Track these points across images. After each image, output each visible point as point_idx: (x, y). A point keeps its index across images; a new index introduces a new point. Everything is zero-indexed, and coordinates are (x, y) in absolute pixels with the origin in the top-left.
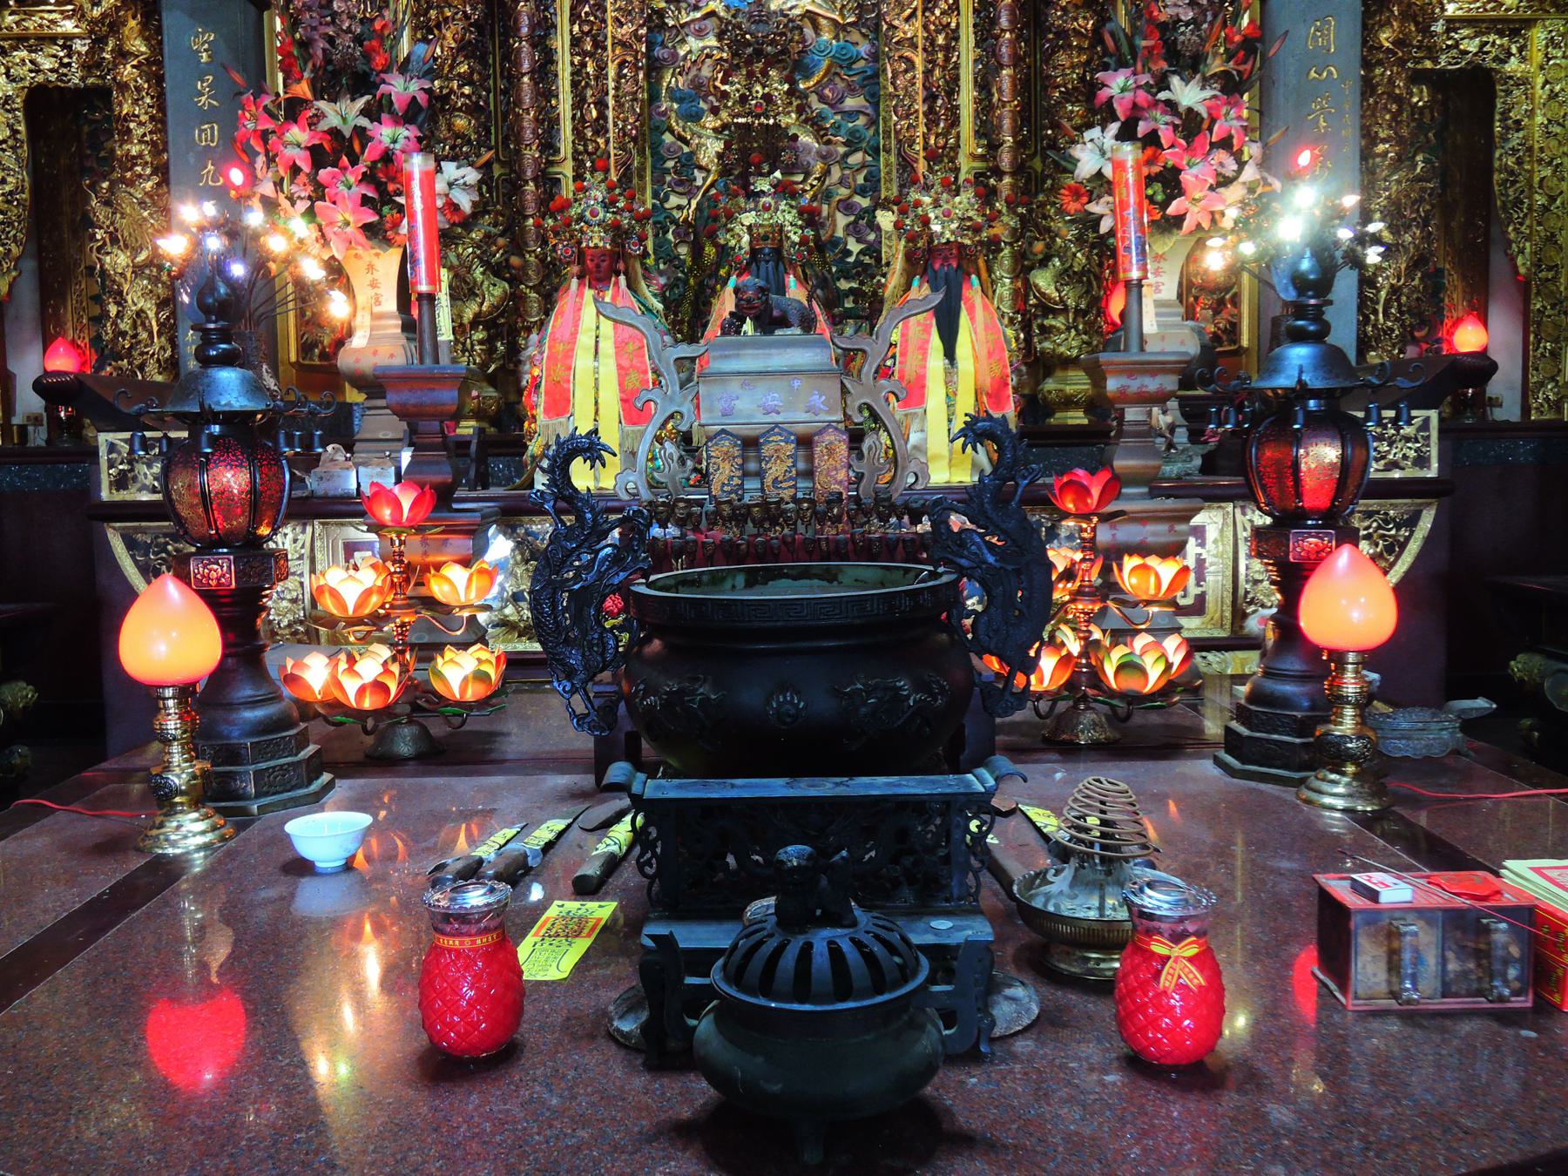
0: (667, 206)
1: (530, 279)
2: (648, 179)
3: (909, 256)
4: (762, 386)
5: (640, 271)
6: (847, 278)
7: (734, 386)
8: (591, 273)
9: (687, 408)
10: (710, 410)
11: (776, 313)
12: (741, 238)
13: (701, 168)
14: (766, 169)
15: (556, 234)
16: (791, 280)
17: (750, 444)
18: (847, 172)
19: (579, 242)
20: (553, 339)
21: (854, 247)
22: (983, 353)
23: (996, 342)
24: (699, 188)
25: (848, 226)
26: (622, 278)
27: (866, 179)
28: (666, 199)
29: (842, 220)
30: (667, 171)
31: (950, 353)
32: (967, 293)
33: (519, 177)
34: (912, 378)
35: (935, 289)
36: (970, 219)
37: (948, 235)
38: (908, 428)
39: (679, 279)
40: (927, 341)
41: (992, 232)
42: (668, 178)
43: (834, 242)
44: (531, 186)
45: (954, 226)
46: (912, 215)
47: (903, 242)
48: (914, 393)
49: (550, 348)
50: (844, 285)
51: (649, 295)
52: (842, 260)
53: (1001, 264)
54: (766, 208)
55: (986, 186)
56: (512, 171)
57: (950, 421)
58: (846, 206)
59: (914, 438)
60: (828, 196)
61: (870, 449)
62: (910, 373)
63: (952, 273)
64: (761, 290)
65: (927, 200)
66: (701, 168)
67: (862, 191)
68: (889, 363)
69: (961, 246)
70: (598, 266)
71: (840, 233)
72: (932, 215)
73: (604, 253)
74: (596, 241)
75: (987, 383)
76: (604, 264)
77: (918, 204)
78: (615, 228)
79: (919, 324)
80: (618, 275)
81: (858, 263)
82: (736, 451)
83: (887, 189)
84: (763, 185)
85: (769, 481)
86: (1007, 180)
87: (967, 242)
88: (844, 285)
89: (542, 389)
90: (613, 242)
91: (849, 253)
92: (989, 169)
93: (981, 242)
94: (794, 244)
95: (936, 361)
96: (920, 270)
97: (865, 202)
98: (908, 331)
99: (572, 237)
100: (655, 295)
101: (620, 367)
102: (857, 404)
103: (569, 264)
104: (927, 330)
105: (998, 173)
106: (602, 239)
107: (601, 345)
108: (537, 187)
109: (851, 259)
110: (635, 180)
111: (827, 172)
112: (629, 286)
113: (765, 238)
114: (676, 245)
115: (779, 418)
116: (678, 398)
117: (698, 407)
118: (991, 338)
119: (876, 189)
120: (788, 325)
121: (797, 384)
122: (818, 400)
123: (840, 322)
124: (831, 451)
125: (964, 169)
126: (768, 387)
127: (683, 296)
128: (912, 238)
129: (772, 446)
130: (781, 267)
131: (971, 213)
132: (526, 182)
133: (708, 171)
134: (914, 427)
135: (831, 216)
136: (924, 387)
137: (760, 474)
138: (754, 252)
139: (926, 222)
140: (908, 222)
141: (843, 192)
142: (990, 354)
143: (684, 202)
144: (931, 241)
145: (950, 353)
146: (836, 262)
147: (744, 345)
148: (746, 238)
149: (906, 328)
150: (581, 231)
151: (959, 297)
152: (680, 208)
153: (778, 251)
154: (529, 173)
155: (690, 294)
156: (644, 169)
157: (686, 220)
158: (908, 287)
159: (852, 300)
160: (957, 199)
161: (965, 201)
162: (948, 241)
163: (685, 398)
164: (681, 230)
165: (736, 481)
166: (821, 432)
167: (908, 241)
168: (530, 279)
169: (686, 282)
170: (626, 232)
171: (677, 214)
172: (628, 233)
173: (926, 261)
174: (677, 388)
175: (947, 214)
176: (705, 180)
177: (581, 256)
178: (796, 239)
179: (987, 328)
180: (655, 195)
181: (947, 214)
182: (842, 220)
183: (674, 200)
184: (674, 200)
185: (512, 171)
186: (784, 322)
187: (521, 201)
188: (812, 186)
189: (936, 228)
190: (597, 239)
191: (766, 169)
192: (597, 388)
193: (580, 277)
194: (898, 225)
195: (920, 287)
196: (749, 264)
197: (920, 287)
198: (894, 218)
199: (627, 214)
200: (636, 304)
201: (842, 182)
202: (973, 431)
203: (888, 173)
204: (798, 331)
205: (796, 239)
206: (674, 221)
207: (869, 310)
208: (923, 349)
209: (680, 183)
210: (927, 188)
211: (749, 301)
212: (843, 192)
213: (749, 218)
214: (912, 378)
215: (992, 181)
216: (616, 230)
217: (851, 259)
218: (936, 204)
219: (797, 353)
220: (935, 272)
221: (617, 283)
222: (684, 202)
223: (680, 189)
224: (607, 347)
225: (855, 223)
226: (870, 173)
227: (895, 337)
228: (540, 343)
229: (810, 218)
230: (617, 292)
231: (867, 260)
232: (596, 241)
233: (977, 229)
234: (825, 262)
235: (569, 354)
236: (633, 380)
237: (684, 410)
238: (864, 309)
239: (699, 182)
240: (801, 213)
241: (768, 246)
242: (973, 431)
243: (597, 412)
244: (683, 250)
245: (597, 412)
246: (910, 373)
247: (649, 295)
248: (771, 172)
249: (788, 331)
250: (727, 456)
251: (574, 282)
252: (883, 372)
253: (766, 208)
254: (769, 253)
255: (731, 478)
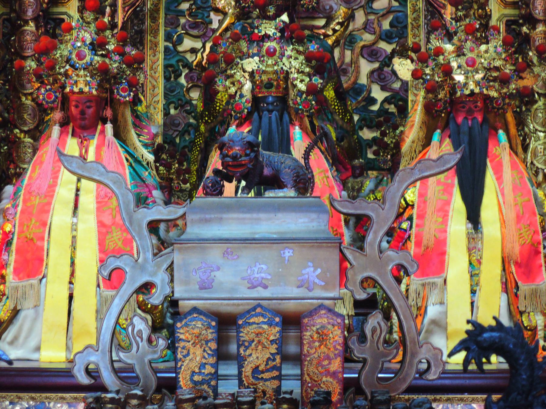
0: (180, 49)
1: (25, 123)
2: (161, 21)
3: (428, 108)
4: (247, 256)
5: (130, 119)
6: (370, 127)
7: (215, 254)
8: (74, 120)
9: (160, 278)
10: (186, 282)
11: (267, 171)
12: (241, 86)
13: (217, 10)
14: (272, 11)
15: (39, 77)
16: (297, 133)
17: (225, 323)
18: (372, 17)
19: (63, 87)
20: (29, 193)
21: (378, 94)
22: (511, 216)
23: (524, 205)
24: (214, 31)
25: (372, 72)
26: (109, 127)
27: (391, 25)
28: (180, 41)
29: (366, 67)
30: (182, 13)
31: (474, 216)
32: (493, 150)
33: (19, 17)
34: (431, 244)
35: (456, 145)
36: (497, 69)
37: (472, 86)
38: (425, 299)
39: (190, 125)
40: (448, 203)
41: (522, 83)
42: (183, 21)
43: (357, 89)
44: (31, 27)
45: (479, 76)
46: (432, 64)
47: (422, 93)
48: (433, 260)
49: (25, 201)
50: (367, 134)
51: (138, 144)
52: (365, 109)
53: (535, 117)
54: (271, 53)
55: (520, 33)
56: (13, 10)
57: (473, 292)
58: (370, 52)
59: (432, 311)
60: (349, 41)
61: (374, 331)
62: (428, 238)
63: (477, 129)
64: (251, 146)
65: (449, 47)
66: (217, 10)
67: (387, 37)
68: (405, 225)
69: (487, 99)
70: (83, 113)
71: (363, 80)
72: (454, 64)
73: (90, 98)
74: (81, 85)
75: (516, 251)
76: (90, 111)
77: (439, 51)
78: (104, 70)
79: (439, 183)
80: (104, 122)
81: (383, 111)
82: (210, 334)
83: (415, 36)
84: (269, 28)
85: (248, 370)
86: (540, 28)
87: (494, 94)
88: (367, 134)
89: (14, 247)
90: (100, 86)
91: (373, 101)
92: (521, 16)
93: (511, 96)
94: (300, 93)
95: (458, 225)
96: (441, 123)
97: (387, 48)
98: (427, 191)
99: (55, 81)
100: (146, 146)
101: (101, 224)
102: (359, 278)
103: (52, 109)
104: (448, 190)
105: (532, 22)
106: (87, 83)
107: (81, 199)
108: (37, 28)
109: (375, 108)
110: (148, 22)
111: (350, 17)
112: (117, 134)
113: (269, 85)
114: (188, 90)
115: (266, 293)
116: (150, 267)
117: (172, 276)
118: (520, 200)
119: (403, 35)
120: (280, 185)
121: (288, 253)
122: (311, 273)
123: (361, 175)
124: (323, 337)
125: (495, 16)
126: (259, 253)
127: (193, 142)
128: (432, 89)
129: (252, 329)
130: (286, 117)
131: (498, 63)
132: (26, 22)
133: (225, 14)
134: (433, 298)
135: (354, 63)
136: (444, 253)
137: (240, 360)
138: (256, 101)
139: (447, 71)
140: (428, 71)
141: (368, 38)
142: (519, 218)
143: (198, 45)
144: (453, 91)
145: (474, 216)
146: (357, 110)
147: (228, 208)
148: (248, 86)
149: (424, 187)
150: (66, 75)
151: (485, 153)
152: (194, 51)
153: (283, 100)
154: (30, 13)
155: (200, 141)
156: (157, 11)
157: (200, 64)
158: (427, 142)
159: (364, 151)
160: (483, 47)
161: (491, 52)
162: (472, 93)
163: (159, 266)
164: (195, 75)
165: (209, 369)
166: (312, 313)
167: (428, 91)
168: (25, 123)
169: (197, 128)
170: (115, 77)
171: (190, 57)
172: (116, 78)
173: (448, 114)
174: (150, 256)
175: (472, 63)
176: (221, 22)
177: (65, 100)
178: (302, 87)
179: (515, 189)
180: (168, 37)
181: (472, 63)
182: (366, 67)
183: (188, 43)
184: (188, 43)
185: (13, 10)
186: (275, 182)
187: (20, 41)
188: (335, 31)
189: (459, 78)
190: (82, 84)
191: (272, 11)
192: (74, 247)
193: (64, 124)
194: (416, 75)
195: (441, 142)
196: (250, 113)
197: (441, 142)
198: (412, 67)
199: (117, 58)
200: (123, 155)
201: (366, 27)
202: (478, 343)
203: (415, 19)
204: (291, 193)
205: (302, 87)
206: (187, 65)
207: (389, 162)
208: (444, 211)
209: (195, 26)
210: (450, 36)
211: (235, 158)
212: (368, 38)
213: (251, 64)
214: (431, 244)
215: (525, 29)
216: (103, 73)
217: (375, 108)
218: (459, 52)
219: (285, 218)
220: (458, 126)
221: (103, 132)
222: (198, 45)
223: (195, 32)
224: (88, 201)
225: (380, 69)
226: (396, 19)
227: (411, 196)
228: (15, 196)
229: (321, 64)
230: (100, 147)
231: (392, 109)
232: (81, 85)
233: (504, 81)
234: (346, 111)
235: (45, 209)
236: (116, 238)
237: (157, 280)
238: (385, 162)
239: (215, 25)
240: (309, 59)
241: (271, 95)
242: (478, 343)
243: (72, 274)
244: (195, 95)
245: (72, 274)
246: (428, 238)
247: (138, 144)
248: (278, 14)
249: (280, 193)
250: (198, 340)
251: (56, 130)
252: (397, 237)
253: (271, 53)
254: (273, 102)
255: (203, 366)
